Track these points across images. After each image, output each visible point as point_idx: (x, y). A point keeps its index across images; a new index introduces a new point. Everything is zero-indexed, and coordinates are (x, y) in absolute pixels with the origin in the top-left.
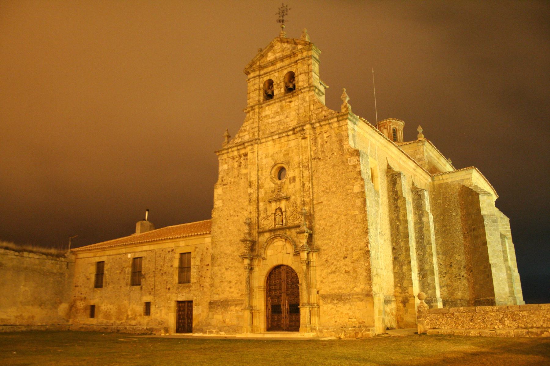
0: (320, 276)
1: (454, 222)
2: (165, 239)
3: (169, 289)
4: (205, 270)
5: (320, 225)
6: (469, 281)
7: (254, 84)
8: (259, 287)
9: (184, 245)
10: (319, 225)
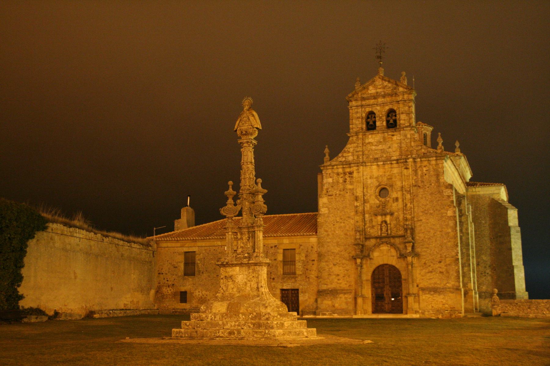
0: (420, 274)
1: (483, 229)
2: (269, 237)
3: (274, 279)
4: (311, 265)
5: (420, 237)
6: (492, 278)
7: (357, 113)
8: (367, 280)
9: (287, 242)
10: (419, 236)
